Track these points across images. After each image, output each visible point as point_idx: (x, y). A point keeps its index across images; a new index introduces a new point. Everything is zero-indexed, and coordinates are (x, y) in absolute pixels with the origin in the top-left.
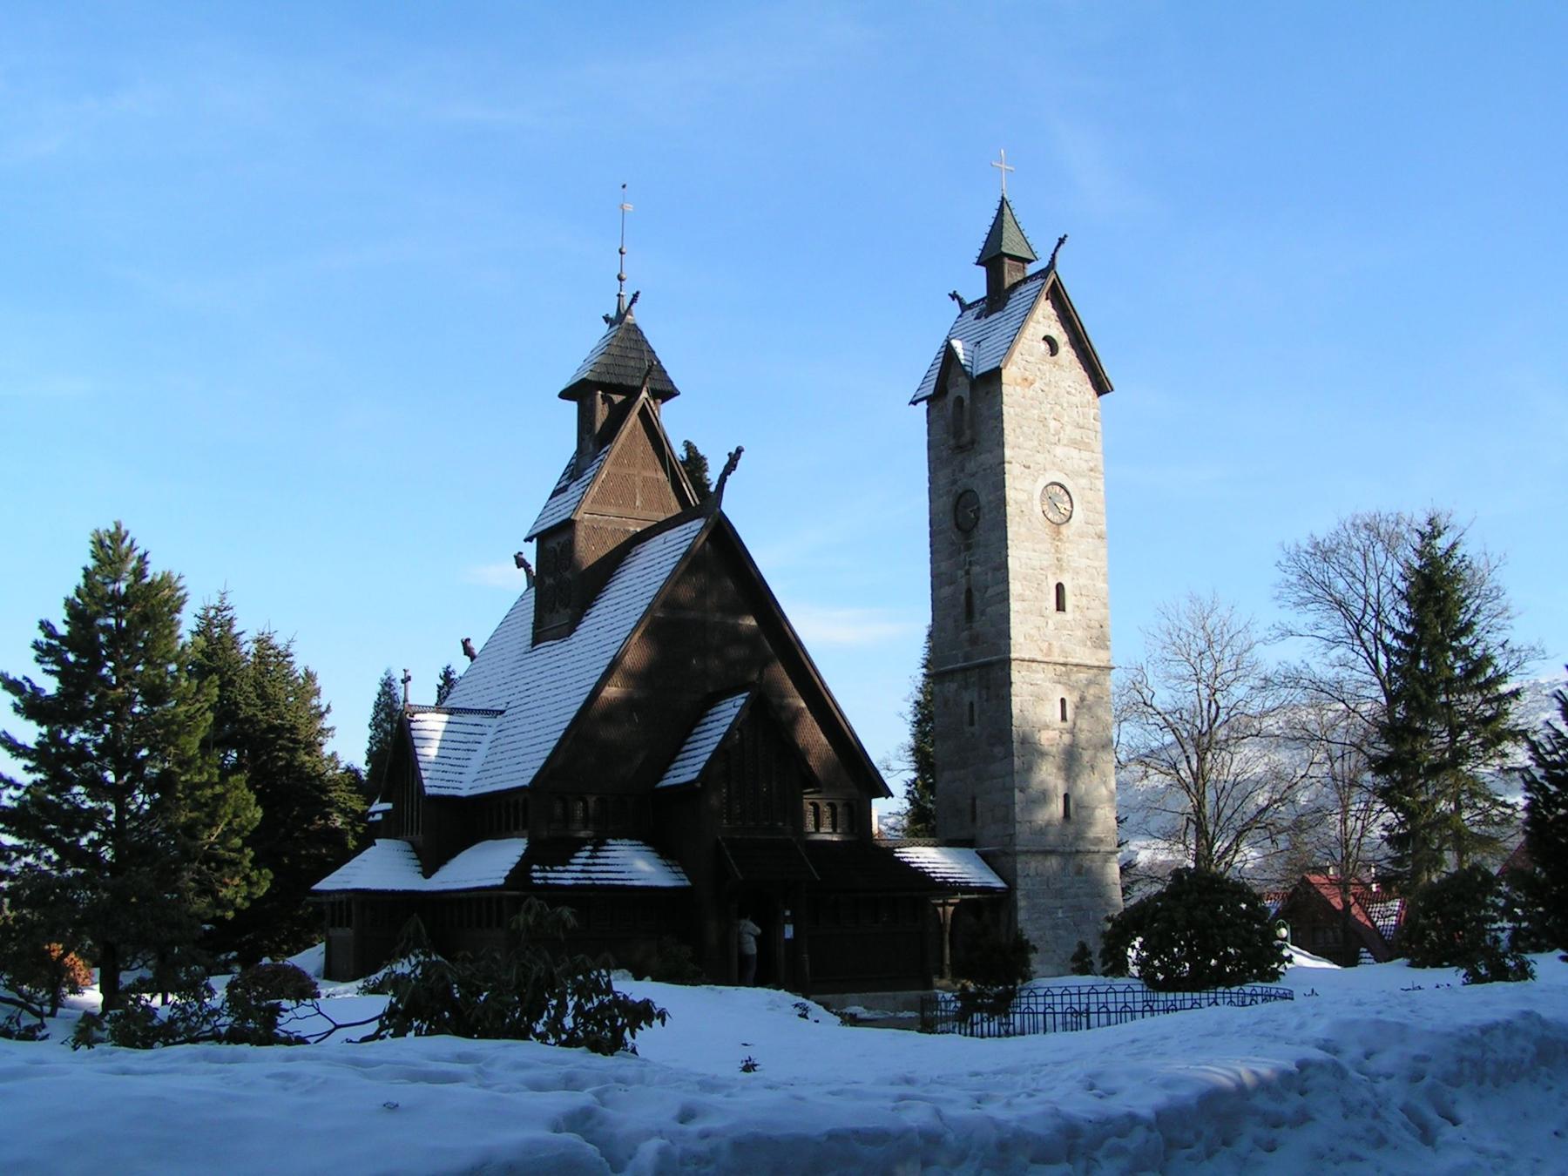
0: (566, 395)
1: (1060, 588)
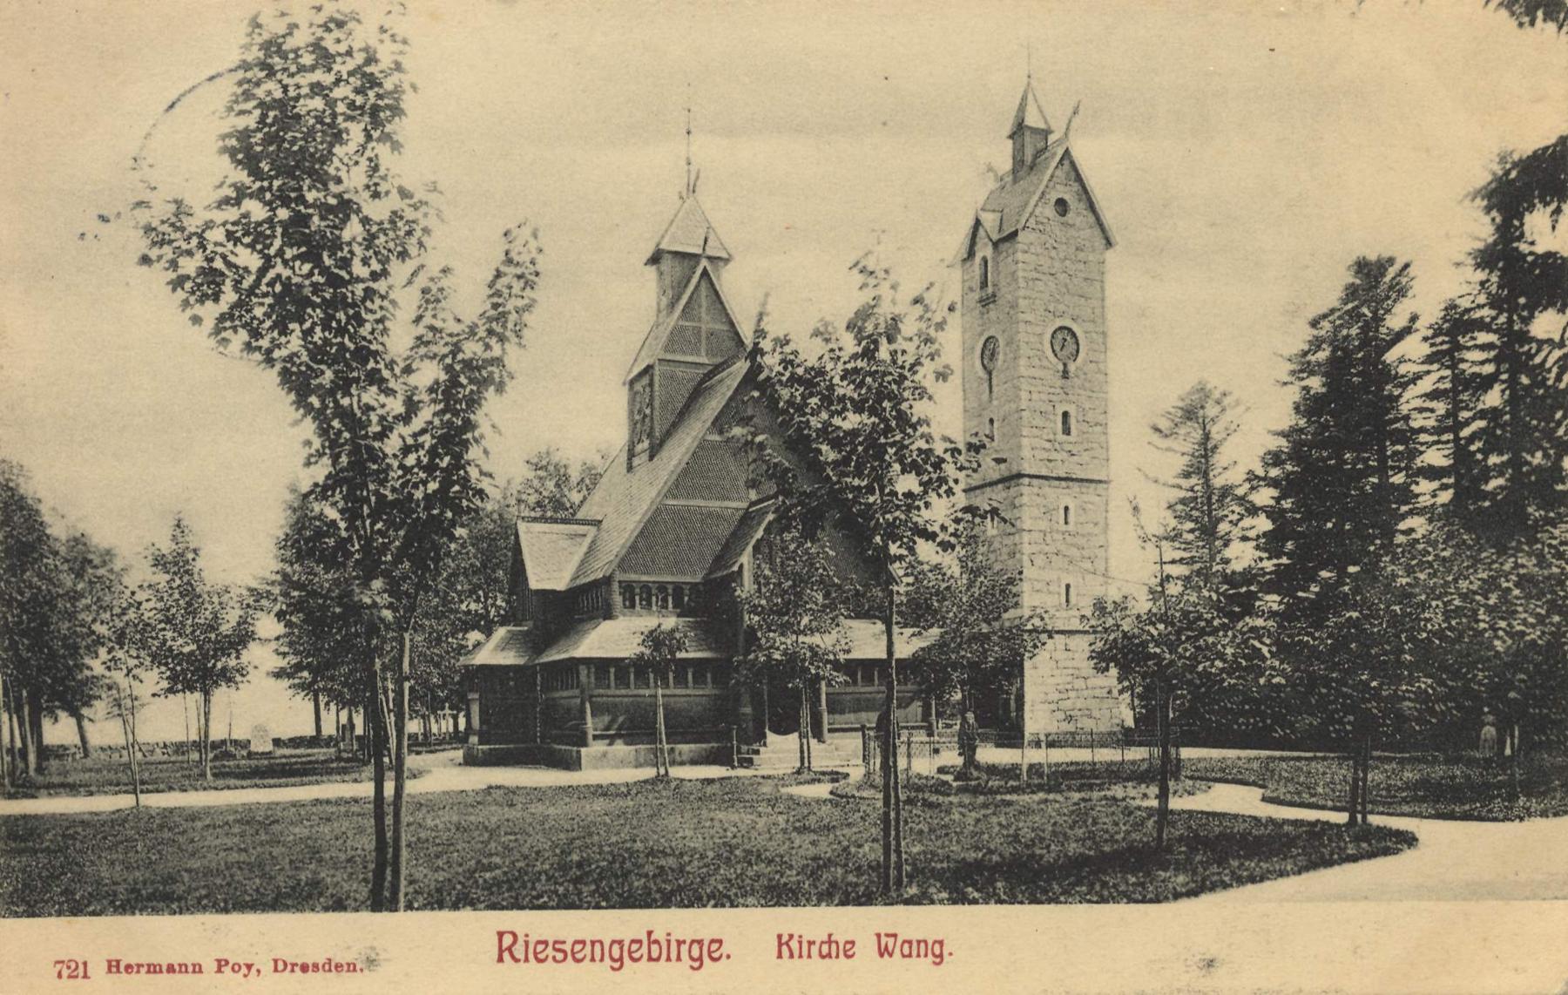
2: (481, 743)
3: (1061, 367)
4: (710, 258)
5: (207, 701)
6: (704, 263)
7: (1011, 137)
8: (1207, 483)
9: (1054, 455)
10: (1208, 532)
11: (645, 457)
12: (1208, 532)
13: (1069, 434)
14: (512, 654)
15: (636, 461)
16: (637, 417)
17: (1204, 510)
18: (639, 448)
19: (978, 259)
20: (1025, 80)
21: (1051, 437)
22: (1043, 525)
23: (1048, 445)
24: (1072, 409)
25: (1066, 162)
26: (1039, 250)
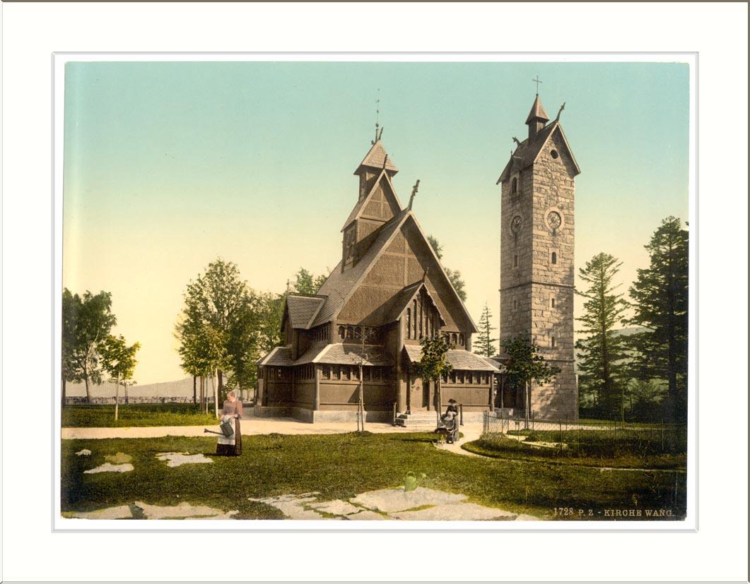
0: (355, 174)
1: (554, 254)
2: (262, 405)
3: (552, 231)
4: (387, 171)
5: (534, 283)
6: (384, 172)
7: (526, 123)
8: (602, 296)
9: (548, 273)
10: (602, 317)
11: (351, 266)
12: (602, 317)
13: (555, 263)
14: (171, 465)
15: (345, 269)
16: (348, 247)
17: (602, 306)
18: (347, 262)
19: (511, 179)
20: (536, 96)
21: (547, 264)
22: (543, 307)
23: (545, 268)
24: (557, 251)
25: (557, 133)
26: (544, 174)
